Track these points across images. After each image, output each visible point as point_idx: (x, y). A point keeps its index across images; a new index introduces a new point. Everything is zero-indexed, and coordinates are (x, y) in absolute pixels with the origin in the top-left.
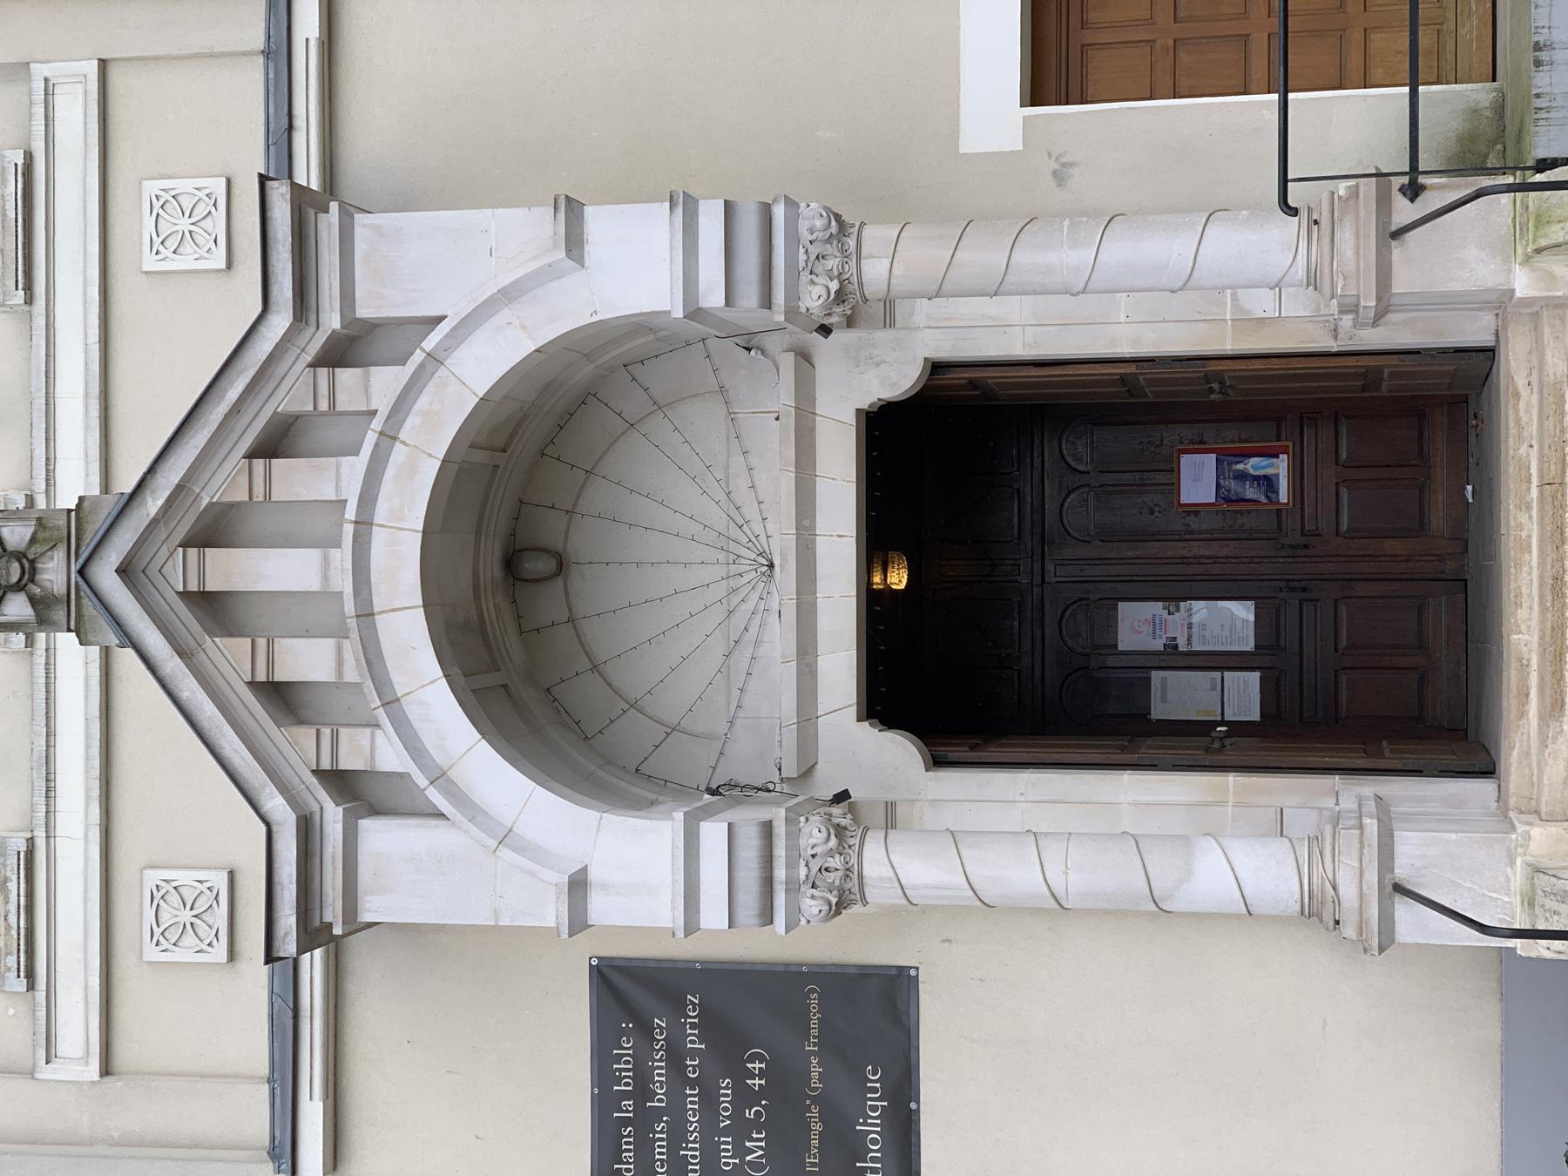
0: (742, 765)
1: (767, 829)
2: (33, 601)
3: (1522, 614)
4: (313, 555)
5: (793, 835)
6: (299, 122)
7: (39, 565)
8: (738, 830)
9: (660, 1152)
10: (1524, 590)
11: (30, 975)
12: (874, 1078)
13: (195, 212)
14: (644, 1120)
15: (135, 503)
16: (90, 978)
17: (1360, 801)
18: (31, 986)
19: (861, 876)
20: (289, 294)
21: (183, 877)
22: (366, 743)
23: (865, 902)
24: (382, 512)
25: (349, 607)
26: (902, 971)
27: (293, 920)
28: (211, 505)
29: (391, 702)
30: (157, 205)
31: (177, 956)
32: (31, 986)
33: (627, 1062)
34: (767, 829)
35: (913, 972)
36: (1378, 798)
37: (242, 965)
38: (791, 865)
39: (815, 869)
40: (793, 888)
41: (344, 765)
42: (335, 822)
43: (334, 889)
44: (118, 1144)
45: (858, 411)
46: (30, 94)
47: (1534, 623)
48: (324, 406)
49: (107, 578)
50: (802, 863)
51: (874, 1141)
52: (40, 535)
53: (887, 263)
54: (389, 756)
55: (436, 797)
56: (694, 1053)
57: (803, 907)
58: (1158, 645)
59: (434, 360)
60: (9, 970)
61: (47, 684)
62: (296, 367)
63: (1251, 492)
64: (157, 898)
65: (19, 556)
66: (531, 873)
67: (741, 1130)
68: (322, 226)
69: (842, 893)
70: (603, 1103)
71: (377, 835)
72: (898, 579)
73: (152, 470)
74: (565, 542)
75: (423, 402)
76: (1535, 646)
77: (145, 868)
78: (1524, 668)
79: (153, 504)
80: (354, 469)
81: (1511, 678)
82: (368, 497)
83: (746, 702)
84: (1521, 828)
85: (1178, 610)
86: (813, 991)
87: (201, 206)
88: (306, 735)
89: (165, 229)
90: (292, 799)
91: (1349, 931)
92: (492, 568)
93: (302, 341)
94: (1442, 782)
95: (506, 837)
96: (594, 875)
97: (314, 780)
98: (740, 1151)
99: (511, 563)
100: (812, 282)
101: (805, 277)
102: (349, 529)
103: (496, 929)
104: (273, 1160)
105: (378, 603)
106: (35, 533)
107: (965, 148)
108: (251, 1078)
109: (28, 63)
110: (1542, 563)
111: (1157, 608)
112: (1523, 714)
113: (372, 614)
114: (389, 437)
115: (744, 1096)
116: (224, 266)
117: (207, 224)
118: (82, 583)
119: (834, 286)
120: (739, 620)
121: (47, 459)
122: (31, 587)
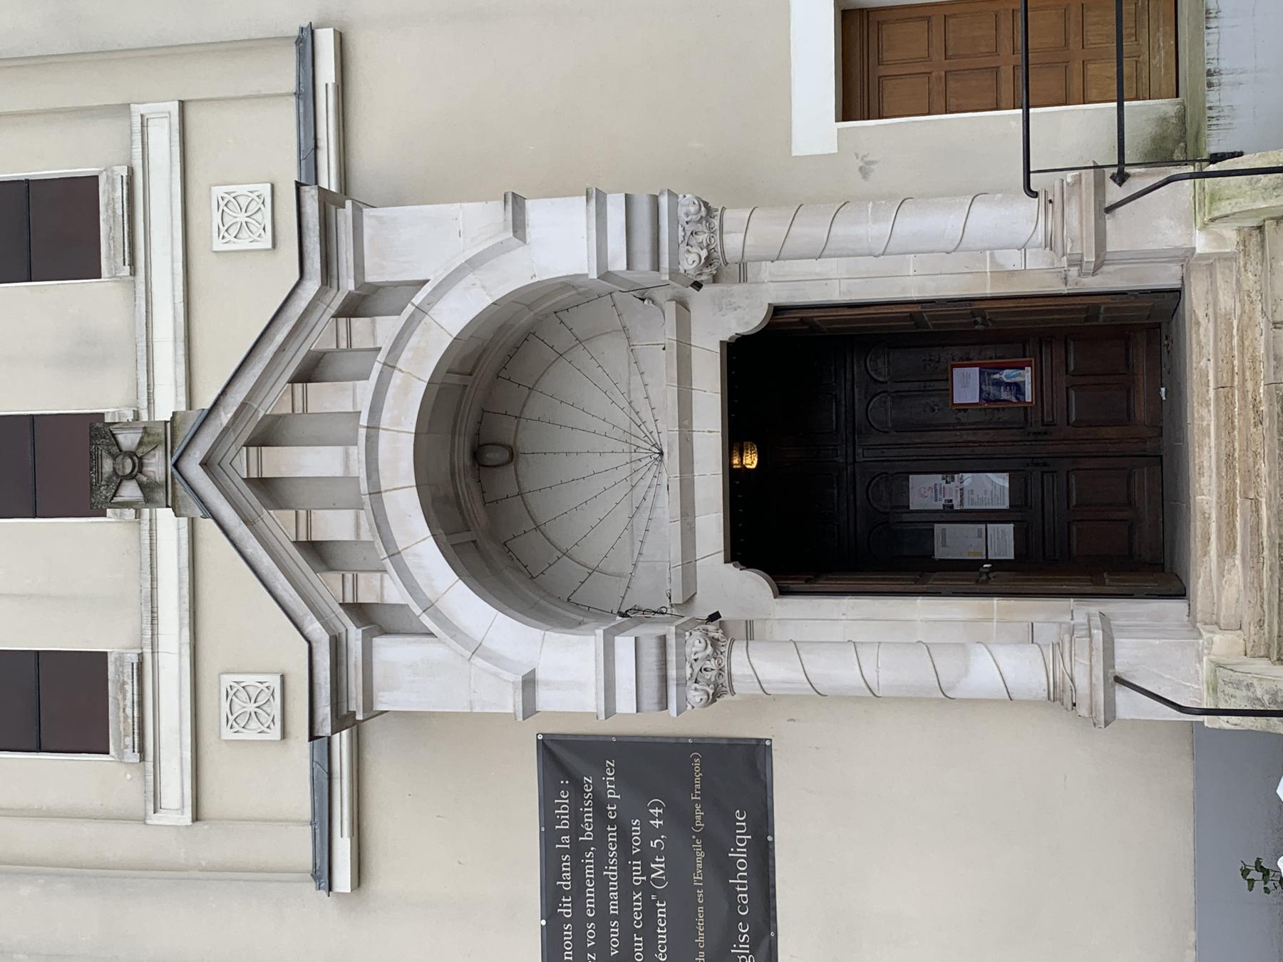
0: (642, 596)
1: (663, 640)
2: (142, 486)
4: (338, 451)
5: (681, 645)
6: (322, 143)
7: (145, 461)
10: (1206, 464)
11: (142, 750)
12: (741, 819)
14: (578, 851)
15: (212, 416)
16: (184, 752)
17: (1089, 616)
18: (143, 759)
19: (730, 674)
21: (249, 680)
22: (377, 583)
25: (364, 487)
26: (760, 742)
27: (328, 710)
28: (265, 416)
29: (394, 554)
30: (222, 203)
32: (143, 759)
34: (663, 640)
35: (768, 743)
37: (291, 742)
38: (680, 667)
39: (697, 670)
40: (681, 683)
41: (363, 599)
46: (131, 126)
47: (1214, 487)
48: (343, 345)
49: (193, 468)
50: (688, 665)
51: (742, 865)
52: (146, 439)
54: (394, 592)
55: (427, 621)
56: (612, 802)
57: (689, 697)
59: (421, 310)
60: (126, 747)
63: (1005, 395)
65: (131, 454)
67: (647, 857)
72: (751, 461)
73: (224, 392)
74: (515, 442)
75: (413, 341)
76: (1214, 504)
77: (222, 673)
78: (1206, 519)
79: (225, 417)
80: (365, 389)
81: (1197, 527)
82: (376, 409)
84: (1206, 635)
87: (254, 203)
88: (334, 578)
90: (326, 625)
92: (464, 459)
96: (540, 676)
99: (477, 454)
100: (688, 251)
102: (362, 432)
106: (142, 438)
109: (129, 104)
110: (1218, 445)
111: (938, 478)
112: (1206, 553)
113: (380, 492)
114: (390, 366)
115: (648, 833)
116: (270, 246)
117: (258, 216)
118: (176, 473)
119: (704, 253)
120: (640, 491)
122: (140, 476)
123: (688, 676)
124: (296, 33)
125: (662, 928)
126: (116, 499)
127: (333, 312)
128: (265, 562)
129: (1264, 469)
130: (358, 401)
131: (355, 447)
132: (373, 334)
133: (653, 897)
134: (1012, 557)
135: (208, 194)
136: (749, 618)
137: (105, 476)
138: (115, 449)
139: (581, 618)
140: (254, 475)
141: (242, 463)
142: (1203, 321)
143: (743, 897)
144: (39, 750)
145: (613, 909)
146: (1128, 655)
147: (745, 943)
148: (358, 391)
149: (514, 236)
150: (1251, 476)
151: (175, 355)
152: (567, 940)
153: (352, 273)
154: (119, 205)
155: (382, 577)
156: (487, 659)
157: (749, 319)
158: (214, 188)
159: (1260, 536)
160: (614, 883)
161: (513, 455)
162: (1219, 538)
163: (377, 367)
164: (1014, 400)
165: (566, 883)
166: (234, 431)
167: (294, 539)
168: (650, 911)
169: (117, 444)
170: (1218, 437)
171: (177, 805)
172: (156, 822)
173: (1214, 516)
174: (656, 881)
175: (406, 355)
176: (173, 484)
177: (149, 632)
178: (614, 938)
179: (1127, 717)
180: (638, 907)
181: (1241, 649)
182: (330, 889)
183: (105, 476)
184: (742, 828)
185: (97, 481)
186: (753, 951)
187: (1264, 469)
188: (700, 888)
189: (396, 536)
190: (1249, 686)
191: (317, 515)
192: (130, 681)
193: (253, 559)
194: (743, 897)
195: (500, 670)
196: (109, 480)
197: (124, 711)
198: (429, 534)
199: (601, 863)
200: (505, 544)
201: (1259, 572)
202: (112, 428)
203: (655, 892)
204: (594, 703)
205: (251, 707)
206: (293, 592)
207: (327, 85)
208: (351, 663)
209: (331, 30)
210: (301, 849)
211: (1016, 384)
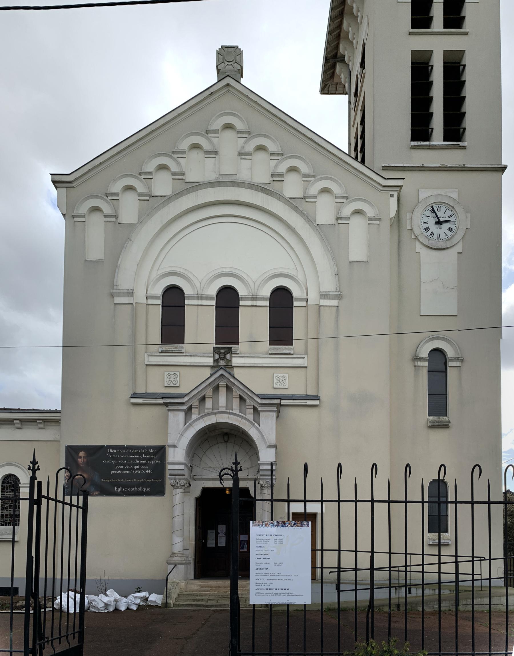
0: (196, 470)
1: (184, 475)
2: (218, 359)
3: (215, 582)
4: (225, 405)
5: (183, 479)
6: (294, 401)
7: (223, 360)
8: (183, 471)
10: (219, 583)
11: (162, 352)
12: (148, 489)
13: (283, 383)
14: (141, 454)
15: (232, 377)
16: (161, 363)
17: (190, 560)
18: (160, 352)
19: (177, 489)
20: (263, 402)
21: (178, 379)
22: (196, 413)
23: (173, 489)
24: (231, 416)
25: (217, 411)
26: (165, 494)
27: (168, 401)
28: (233, 389)
29: (202, 417)
30: (284, 376)
31: (165, 377)
32: (160, 352)
33: (150, 451)
34: (184, 475)
35: (164, 495)
36: (191, 563)
37: (164, 388)
38: (178, 479)
39: (178, 482)
40: (175, 479)
41: (193, 409)
42: (184, 408)
43: (174, 408)
44: (135, 367)
45: (248, 488)
46: (303, 355)
47: (214, 584)
48: (247, 407)
49: (221, 372)
50: (179, 480)
51: (139, 489)
52: (228, 361)
53: (266, 493)
54: (194, 417)
55: (188, 424)
56: (151, 462)
57: (172, 480)
58: (219, 531)
59: (254, 425)
60: (162, 349)
61: (209, 356)
62: (253, 403)
63: (242, 545)
64: (175, 374)
65: (225, 357)
66: (176, 439)
67: (140, 469)
68: (274, 407)
69: (175, 486)
70: (144, 447)
71: (182, 415)
72: (227, 492)
73: (237, 380)
74: (229, 442)
75: (247, 423)
76: (211, 584)
77: (179, 372)
78: (208, 583)
79: (232, 380)
80: (237, 412)
81: (207, 581)
83: (205, 470)
84: (184, 582)
85: (224, 534)
86: (161, 480)
87: (283, 383)
88: (197, 403)
89: (280, 377)
90: (187, 401)
91: (170, 559)
92: (225, 431)
93: (257, 404)
94: (193, 571)
95: (182, 435)
96: (176, 448)
97: (190, 405)
98: (137, 469)
99: (227, 434)
100: (264, 482)
101: (265, 481)
102: (228, 411)
103: (168, 433)
104: (133, 394)
105: (217, 415)
106: (228, 360)
108: (146, 390)
109: (307, 354)
110: (222, 585)
111: (225, 531)
112: (201, 582)
113: (215, 414)
114: (242, 417)
115: (145, 470)
116: (274, 387)
117: (281, 385)
118: (220, 368)
119: (263, 485)
121: (244, 357)
122: (220, 359)
123: (177, 480)
124: (319, 395)
125: (125, 472)
126: (215, 353)
127: (254, 405)
128: (200, 388)
129: (216, 593)
130: (235, 410)
131: (225, 409)
133: (131, 470)
134: (208, 546)
135: (285, 373)
136: (190, 492)
137: (220, 350)
138: (226, 353)
139: (190, 456)
140: (220, 385)
141: (222, 383)
142: (246, 583)
143: (132, 490)
144: (162, 326)
145: (129, 461)
146: (181, 567)
147: (122, 490)
148: (237, 410)
149: (268, 446)
150: (215, 590)
151: (251, 364)
152: (122, 451)
153: (262, 410)
154: (285, 351)
155: (197, 414)
156: (180, 437)
158: (287, 374)
159: (203, 592)
160: (134, 462)
161: (226, 442)
162: (204, 585)
163: (242, 415)
164: (241, 547)
165: (134, 451)
166: (229, 382)
167: (206, 394)
169: (227, 354)
170: (224, 585)
171: (149, 360)
172: (145, 355)
173: (208, 584)
174: (135, 471)
175: (244, 421)
176: (218, 367)
177: (189, 355)
178: (123, 462)
179: (168, 567)
180: (129, 467)
181: (182, 588)
182: (131, 398)
183: (220, 350)
184: (146, 490)
185: (219, 349)
186: (121, 491)
187: (216, 593)
188: (134, 480)
189: (206, 418)
190: (173, 588)
191: (211, 400)
192: (177, 350)
193: (201, 385)
194: (132, 490)
195: (177, 440)
196: (219, 352)
197: (171, 348)
198: (206, 425)
199: (139, 459)
200: (207, 439)
201: (196, 591)
202: (231, 353)
203: (133, 471)
204: (170, 460)
205: (172, 379)
206: (194, 394)
207: (307, 402)
208: (179, 407)
209: (318, 404)
210: (141, 390)
211: (244, 548)
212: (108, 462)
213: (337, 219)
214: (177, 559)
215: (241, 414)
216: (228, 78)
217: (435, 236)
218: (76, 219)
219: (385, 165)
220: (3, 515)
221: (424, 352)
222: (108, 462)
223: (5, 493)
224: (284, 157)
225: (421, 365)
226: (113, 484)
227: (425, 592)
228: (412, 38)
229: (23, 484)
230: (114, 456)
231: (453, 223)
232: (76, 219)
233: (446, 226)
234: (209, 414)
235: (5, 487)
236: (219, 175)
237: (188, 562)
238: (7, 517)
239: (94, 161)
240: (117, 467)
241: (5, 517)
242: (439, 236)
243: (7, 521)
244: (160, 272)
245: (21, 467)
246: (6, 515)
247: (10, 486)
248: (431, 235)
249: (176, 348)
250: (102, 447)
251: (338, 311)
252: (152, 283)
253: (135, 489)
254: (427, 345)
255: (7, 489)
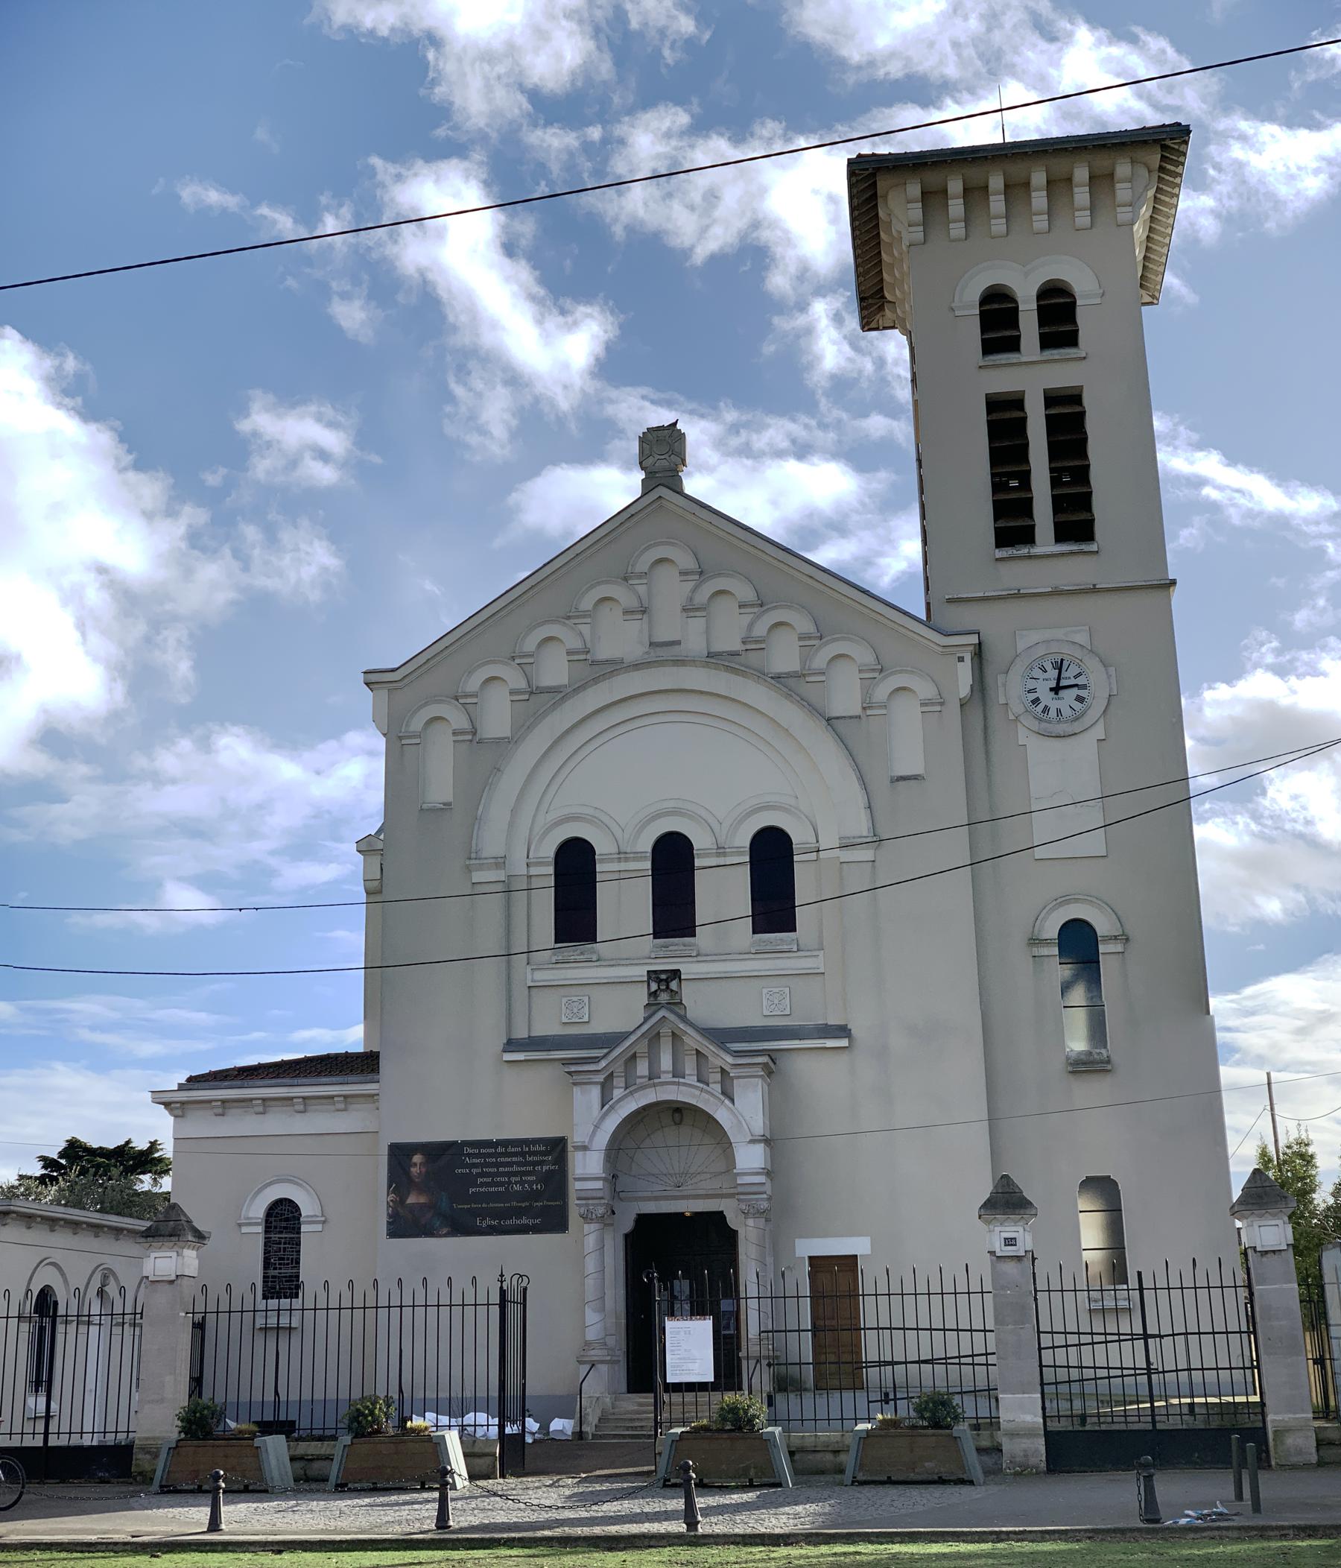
2: (656, 991)
9: (514, 1159)
12: (537, 1221)
14: (523, 1154)
34: (602, 1198)
38: (593, 1205)
40: (587, 1205)
48: (710, 1070)
54: (617, 1093)
65: (668, 987)
67: (522, 1183)
88: (622, 1069)
95: (597, 1127)
98: (516, 1183)
107: (797, 1240)
114: (702, 1090)
115: (531, 1183)
132: (715, 1083)
143: (508, 1222)
145: (501, 1169)
146: (603, 1368)
157: (733, 1221)
160: (511, 1169)
165: (510, 1149)
168: (501, 1184)
169: (672, 980)
175: (707, 1096)
194: (508, 1222)
199: (519, 1164)
210: (521, 1033)
212: (463, 1171)
213: (864, 709)
214: (596, 1354)
215: (699, 1084)
216: (660, 487)
217: (1053, 713)
218: (403, 742)
219: (950, 597)
220: (268, 1277)
221: (1052, 930)
222: (463, 1171)
223: (272, 1236)
224: (765, 608)
225: (1046, 954)
226: (475, 1213)
227: (1074, 1404)
228: (984, 373)
229: (307, 1216)
230: (475, 1161)
231: (1084, 687)
232: (403, 742)
233: (1069, 695)
234: (643, 1087)
235: (271, 1222)
236: (651, 644)
237: (615, 1358)
238: (275, 1282)
239: (437, 644)
240: (480, 1180)
241: (272, 1282)
242: (1059, 712)
243: (275, 1288)
244: (553, 816)
245: (304, 1184)
246: (273, 1277)
247: (281, 1220)
248: (1043, 712)
249: (582, 953)
250: (455, 1143)
251: (874, 867)
252: (536, 839)
253: (513, 1221)
254: (1055, 914)
255: (276, 1227)
